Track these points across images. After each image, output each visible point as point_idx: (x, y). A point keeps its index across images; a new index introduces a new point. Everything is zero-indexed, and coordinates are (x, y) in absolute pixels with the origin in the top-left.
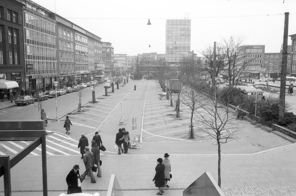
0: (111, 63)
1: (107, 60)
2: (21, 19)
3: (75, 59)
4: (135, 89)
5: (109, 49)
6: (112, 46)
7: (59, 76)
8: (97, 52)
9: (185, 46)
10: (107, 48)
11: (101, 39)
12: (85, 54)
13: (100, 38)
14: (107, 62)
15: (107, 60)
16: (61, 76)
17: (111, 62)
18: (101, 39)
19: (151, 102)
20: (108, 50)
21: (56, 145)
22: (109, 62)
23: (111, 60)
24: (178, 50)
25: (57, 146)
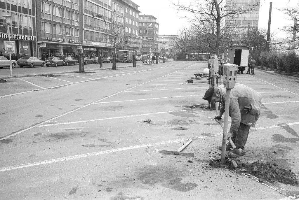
0: (153, 42)
1: (149, 38)
2: (29, 90)
3: (82, 22)
4: (289, 2)
5: (152, 24)
6: (157, 21)
7: (39, 42)
8: (134, 24)
9: (251, 19)
10: (150, 23)
11: (138, 7)
12: (104, 19)
13: (138, 6)
14: (149, 40)
15: (149, 38)
16: (42, 42)
17: (153, 40)
18: (138, 7)
19: (177, 75)
20: (150, 25)
21: (297, 125)
22: (152, 40)
23: (154, 38)
24: (241, 26)
25: (32, 46)
